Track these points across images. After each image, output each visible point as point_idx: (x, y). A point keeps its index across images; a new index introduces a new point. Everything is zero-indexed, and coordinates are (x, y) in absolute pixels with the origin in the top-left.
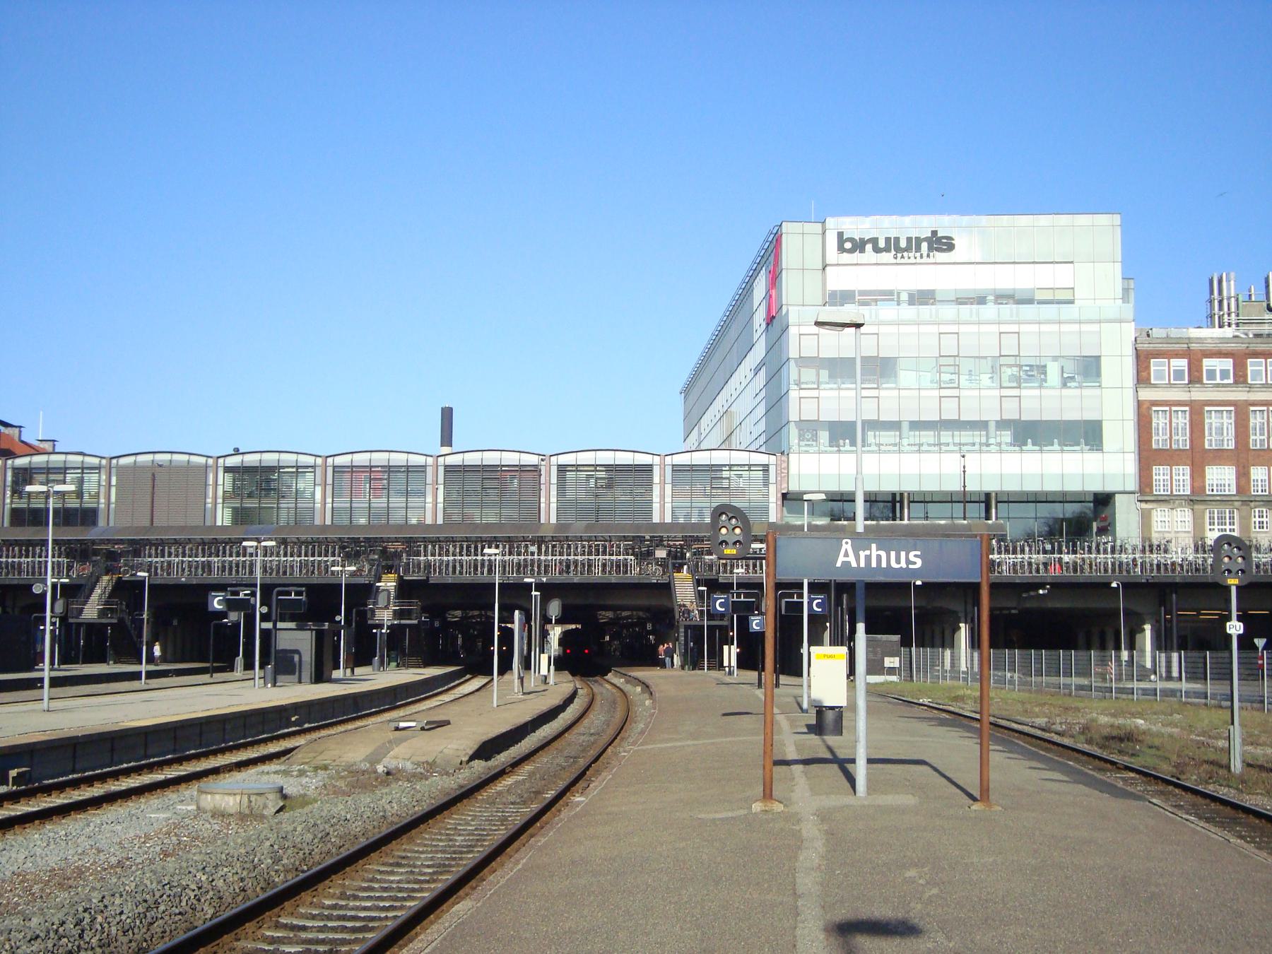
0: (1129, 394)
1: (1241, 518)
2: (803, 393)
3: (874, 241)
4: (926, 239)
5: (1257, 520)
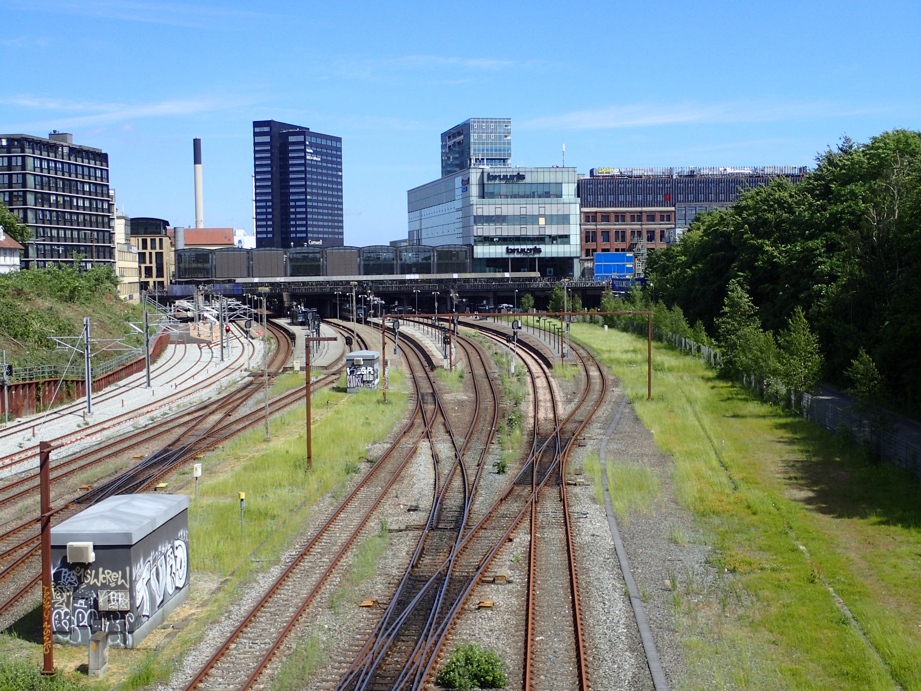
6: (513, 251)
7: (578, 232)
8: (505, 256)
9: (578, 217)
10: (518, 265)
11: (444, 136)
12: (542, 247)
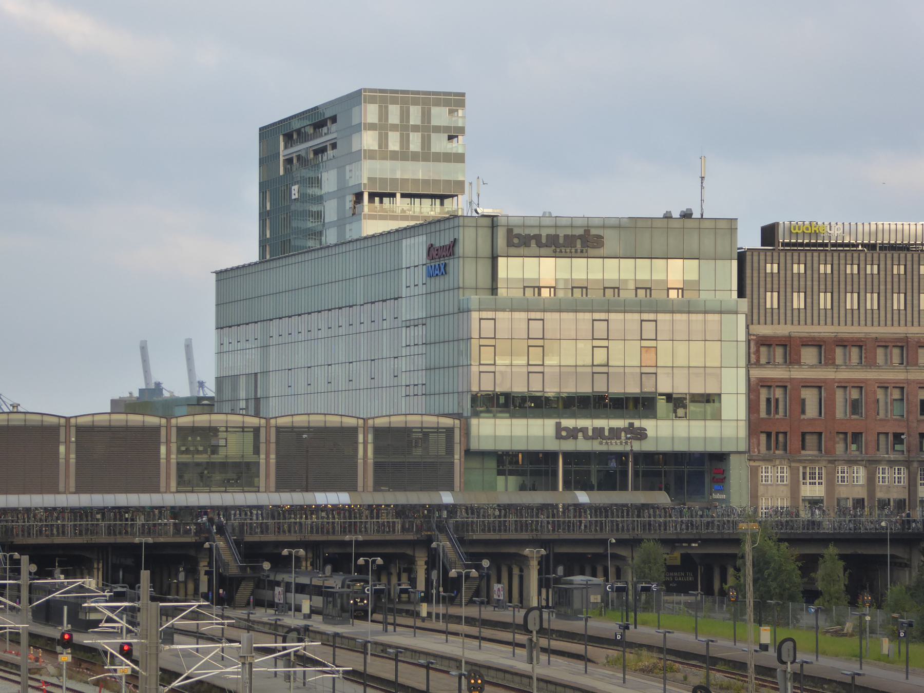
0: (742, 372)
1: (827, 474)
2: (483, 368)
3: (537, 238)
4: (580, 237)
5: (840, 475)
6: (573, 434)
7: (743, 388)
8: (552, 445)
9: (743, 347)
10: (585, 469)
11: (267, 133)
12: (648, 425)
